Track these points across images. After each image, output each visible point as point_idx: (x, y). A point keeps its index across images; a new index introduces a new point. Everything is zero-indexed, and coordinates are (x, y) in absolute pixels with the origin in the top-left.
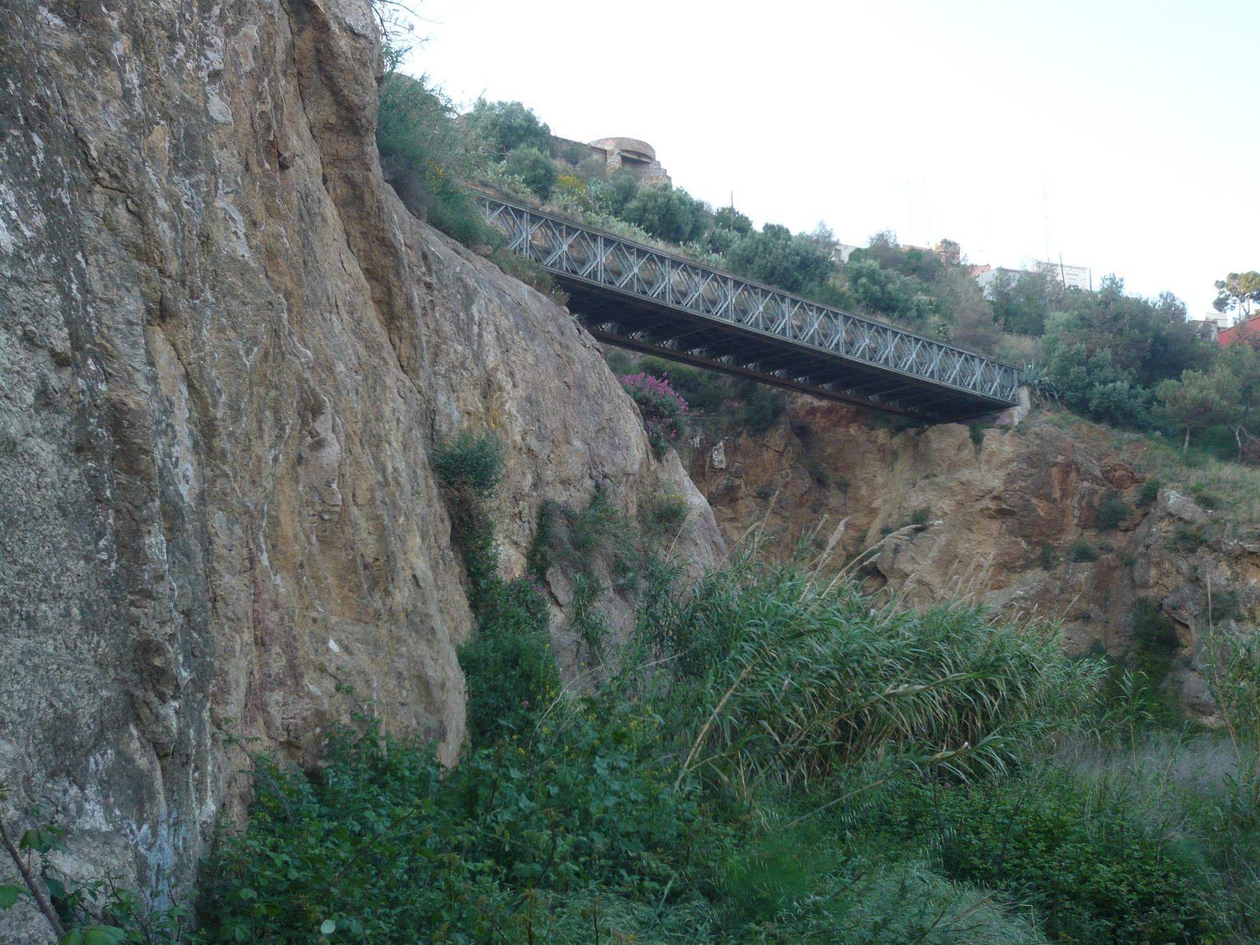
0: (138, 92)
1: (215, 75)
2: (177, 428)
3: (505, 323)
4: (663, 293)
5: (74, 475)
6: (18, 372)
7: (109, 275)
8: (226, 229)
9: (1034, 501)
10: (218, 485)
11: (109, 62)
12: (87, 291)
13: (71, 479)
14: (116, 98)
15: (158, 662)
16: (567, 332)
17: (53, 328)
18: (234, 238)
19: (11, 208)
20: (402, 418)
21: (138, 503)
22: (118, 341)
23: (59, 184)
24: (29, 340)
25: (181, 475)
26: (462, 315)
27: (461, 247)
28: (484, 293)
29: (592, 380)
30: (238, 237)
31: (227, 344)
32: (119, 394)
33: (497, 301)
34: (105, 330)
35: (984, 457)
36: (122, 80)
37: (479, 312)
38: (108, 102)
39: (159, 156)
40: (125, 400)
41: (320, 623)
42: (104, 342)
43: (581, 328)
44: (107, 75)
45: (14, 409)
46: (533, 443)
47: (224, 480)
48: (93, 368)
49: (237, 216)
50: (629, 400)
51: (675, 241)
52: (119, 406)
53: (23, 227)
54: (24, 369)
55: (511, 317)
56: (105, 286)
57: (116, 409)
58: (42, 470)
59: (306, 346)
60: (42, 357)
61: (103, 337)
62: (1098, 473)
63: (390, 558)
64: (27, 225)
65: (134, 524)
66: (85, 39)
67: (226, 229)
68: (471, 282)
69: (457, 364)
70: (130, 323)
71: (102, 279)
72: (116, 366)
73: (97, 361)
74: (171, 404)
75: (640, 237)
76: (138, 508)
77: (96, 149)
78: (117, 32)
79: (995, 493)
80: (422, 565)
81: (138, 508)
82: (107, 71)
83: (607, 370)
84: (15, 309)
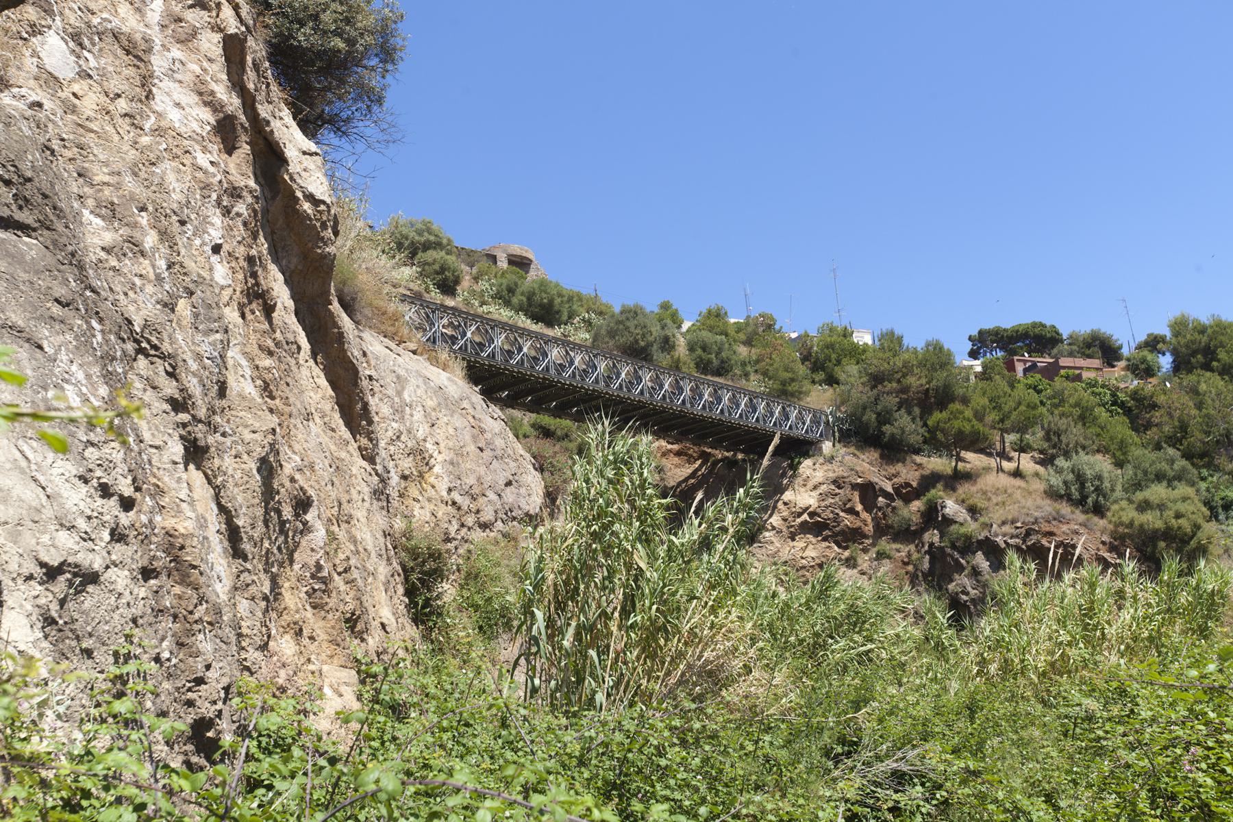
0: (166, 274)
1: (216, 249)
2: (211, 539)
3: (430, 403)
4: (547, 368)
5: (142, 592)
6: (97, 517)
7: (154, 424)
8: (236, 373)
9: (842, 514)
10: (242, 578)
11: (143, 254)
12: (141, 441)
13: (141, 596)
14: (150, 282)
15: (210, 734)
16: (478, 407)
17: (120, 477)
18: (242, 380)
19: (82, 385)
20: (366, 498)
21: (191, 608)
22: (166, 479)
23: (114, 359)
24: (105, 491)
25: (216, 577)
26: (397, 399)
27: (393, 345)
28: (413, 381)
29: (499, 443)
30: (246, 379)
31: (243, 466)
32: (170, 523)
33: (423, 387)
34: (155, 470)
35: (799, 480)
36: (153, 266)
37: (410, 396)
38: (144, 285)
39: (184, 323)
40: (177, 527)
41: (316, 674)
42: (155, 480)
43: (489, 403)
44: (141, 264)
45: (96, 548)
46: (456, 496)
47: (246, 574)
48: (150, 503)
49: (244, 362)
50: (528, 456)
51: (550, 324)
52: (172, 532)
53: (92, 399)
54: (101, 514)
55: (434, 399)
56: (153, 434)
57: (171, 536)
58: (120, 594)
59: (294, 452)
60: (113, 501)
61: (155, 477)
62: (890, 489)
63: (365, 611)
64: (95, 396)
65: (188, 625)
66: (121, 236)
67: (236, 373)
68: (402, 372)
69: (394, 438)
70: (175, 463)
71: (150, 429)
72: (167, 500)
73: (152, 496)
74: (206, 521)
75: (524, 322)
76: (191, 613)
77: (139, 325)
78: (147, 228)
79: (811, 509)
80: (386, 614)
81: (191, 613)
82: (141, 260)
83: (511, 435)
84: (91, 466)
